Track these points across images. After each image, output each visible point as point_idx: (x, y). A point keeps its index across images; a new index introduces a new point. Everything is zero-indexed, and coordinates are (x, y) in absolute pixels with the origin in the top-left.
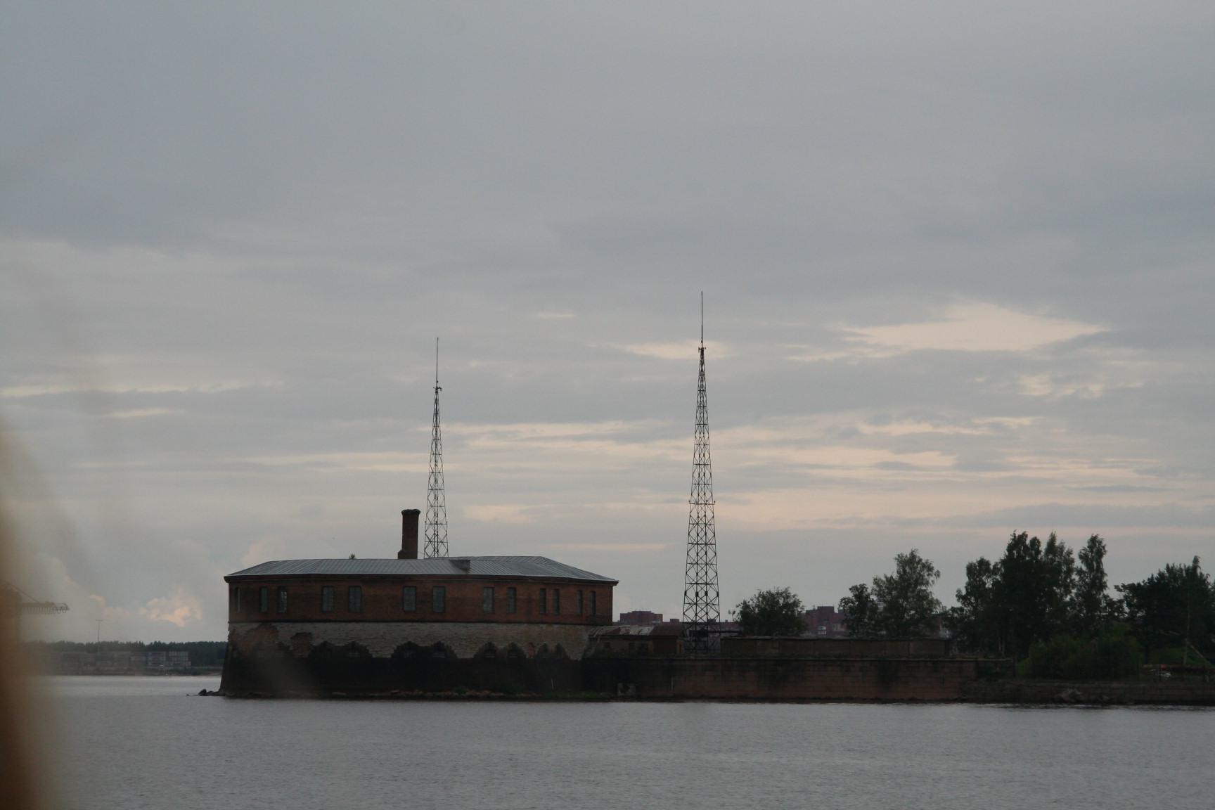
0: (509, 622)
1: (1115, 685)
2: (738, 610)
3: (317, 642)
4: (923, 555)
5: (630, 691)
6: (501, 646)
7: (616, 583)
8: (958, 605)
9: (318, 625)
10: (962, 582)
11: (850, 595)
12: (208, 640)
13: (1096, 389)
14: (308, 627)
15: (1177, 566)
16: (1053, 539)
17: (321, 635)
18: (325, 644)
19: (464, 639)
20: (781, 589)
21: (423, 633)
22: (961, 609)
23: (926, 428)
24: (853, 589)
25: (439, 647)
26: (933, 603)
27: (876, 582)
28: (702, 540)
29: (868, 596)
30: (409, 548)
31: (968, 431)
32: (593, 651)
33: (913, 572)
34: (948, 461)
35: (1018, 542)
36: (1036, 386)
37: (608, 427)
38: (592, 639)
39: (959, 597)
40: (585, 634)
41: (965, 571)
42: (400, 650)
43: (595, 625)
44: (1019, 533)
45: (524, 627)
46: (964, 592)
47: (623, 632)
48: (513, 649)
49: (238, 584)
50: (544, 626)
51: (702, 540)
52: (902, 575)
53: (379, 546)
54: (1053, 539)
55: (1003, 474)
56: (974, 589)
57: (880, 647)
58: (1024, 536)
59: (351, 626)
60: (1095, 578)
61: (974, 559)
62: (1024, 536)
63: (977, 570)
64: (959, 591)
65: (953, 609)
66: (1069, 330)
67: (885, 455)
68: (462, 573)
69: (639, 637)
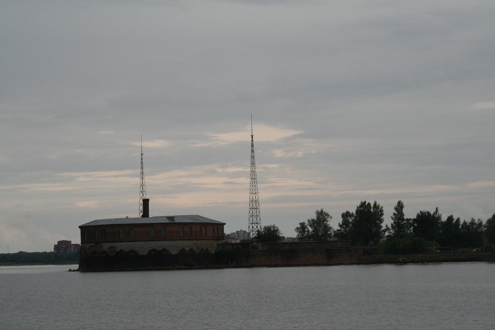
0: (190, 240)
1: (419, 255)
3: (118, 250)
4: (325, 210)
5: (234, 264)
6: (187, 249)
7: (225, 224)
8: (339, 228)
10: (340, 220)
11: (299, 226)
12: (41, 251)
13: (300, 154)
14: (114, 244)
15: (424, 211)
16: (375, 203)
17: (110, 248)
18: (121, 250)
19: (173, 246)
20: (272, 225)
22: (340, 230)
23: (241, 169)
24: (300, 224)
25: (164, 250)
26: (330, 228)
27: (309, 221)
28: (254, 206)
29: (306, 226)
32: (218, 250)
33: (322, 217)
35: (363, 204)
36: (279, 153)
37: (127, 172)
38: (218, 245)
39: (340, 225)
40: (215, 243)
41: (341, 216)
42: (150, 252)
43: (219, 240)
44: (363, 201)
45: (195, 242)
46: (341, 224)
47: (229, 242)
48: (192, 250)
49: (83, 228)
51: (254, 206)
52: (318, 218)
53: (135, 213)
54: (375, 203)
55: (268, 185)
56: (345, 223)
58: (365, 202)
59: (131, 243)
60: (401, 216)
61: (345, 212)
62: (365, 202)
63: (346, 215)
64: (339, 223)
65: (338, 230)
67: (226, 179)
69: (235, 244)
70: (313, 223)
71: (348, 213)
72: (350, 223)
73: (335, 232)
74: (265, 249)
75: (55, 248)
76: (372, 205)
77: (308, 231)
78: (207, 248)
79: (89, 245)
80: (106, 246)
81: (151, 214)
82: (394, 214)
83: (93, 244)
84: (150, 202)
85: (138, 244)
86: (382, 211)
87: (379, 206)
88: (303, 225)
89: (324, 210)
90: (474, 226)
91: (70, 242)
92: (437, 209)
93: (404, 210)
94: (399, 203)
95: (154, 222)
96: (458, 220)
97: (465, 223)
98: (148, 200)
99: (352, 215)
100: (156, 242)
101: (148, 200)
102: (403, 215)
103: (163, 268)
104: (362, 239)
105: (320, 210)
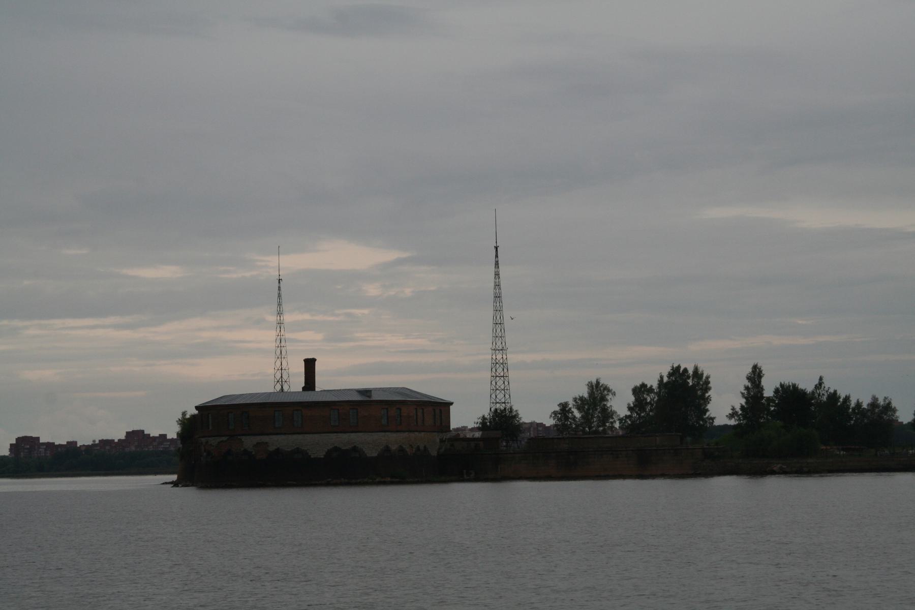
0: (397, 431)
2: (480, 420)
3: (272, 448)
6: (394, 448)
7: (452, 404)
8: (629, 413)
9: (271, 437)
10: (631, 399)
11: (558, 409)
13: (408, 292)
14: (265, 439)
15: (787, 383)
17: (238, 446)
18: (278, 449)
19: (370, 443)
21: (344, 440)
23: (307, 317)
25: (355, 449)
27: (575, 400)
30: (310, 383)
31: (331, 318)
33: (597, 395)
34: (319, 336)
35: (676, 372)
36: (372, 290)
37: (112, 320)
38: (442, 441)
39: (630, 408)
40: (437, 437)
41: (631, 392)
42: (329, 453)
45: (406, 434)
48: (401, 449)
50: (417, 433)
51: (281, 381)
52: (591, 394)
55: (352, 344)
56: (639, 404)
57: (582, 445)
58: (679, 367)
59: (295, 437)
61: (638, 384)
62: (679, 367)
63: (640, 391)
64: (629, 404)
65: (626, 417)
66: (392, 255)
68: (368, 399)
69: (474, 439)
70: (581, 403)
71: (643, 385)
72: (647, 403)
73: (621, 420)
74: (502, 450)
75: (11, 450)
76: (691, 372)
77: (574, 418)
78: (425, 447)
79: (219, 439)
80: (249, 442)
81: (322, 383)
82: (747, 388)
83: (224, 439)
84: (318, 367)
85: (309, 437)
86: (707, 382)
87: (702, 374)
88: (564, 407)
89: (602, 382)
90: (877, 410)
91: (38, 438)
92: (821, 379)
93: (764, 382)
94: (755, 367)
95: (336, 399)
96: (847, 399)
97: (859, 405)
98: (314, 360)
99: (651, 390)
100: (340, 435)
101: (314, 360)
102: (762, 389)
103: (354, 481)
104: (665, 434)
105: (594, 381)
